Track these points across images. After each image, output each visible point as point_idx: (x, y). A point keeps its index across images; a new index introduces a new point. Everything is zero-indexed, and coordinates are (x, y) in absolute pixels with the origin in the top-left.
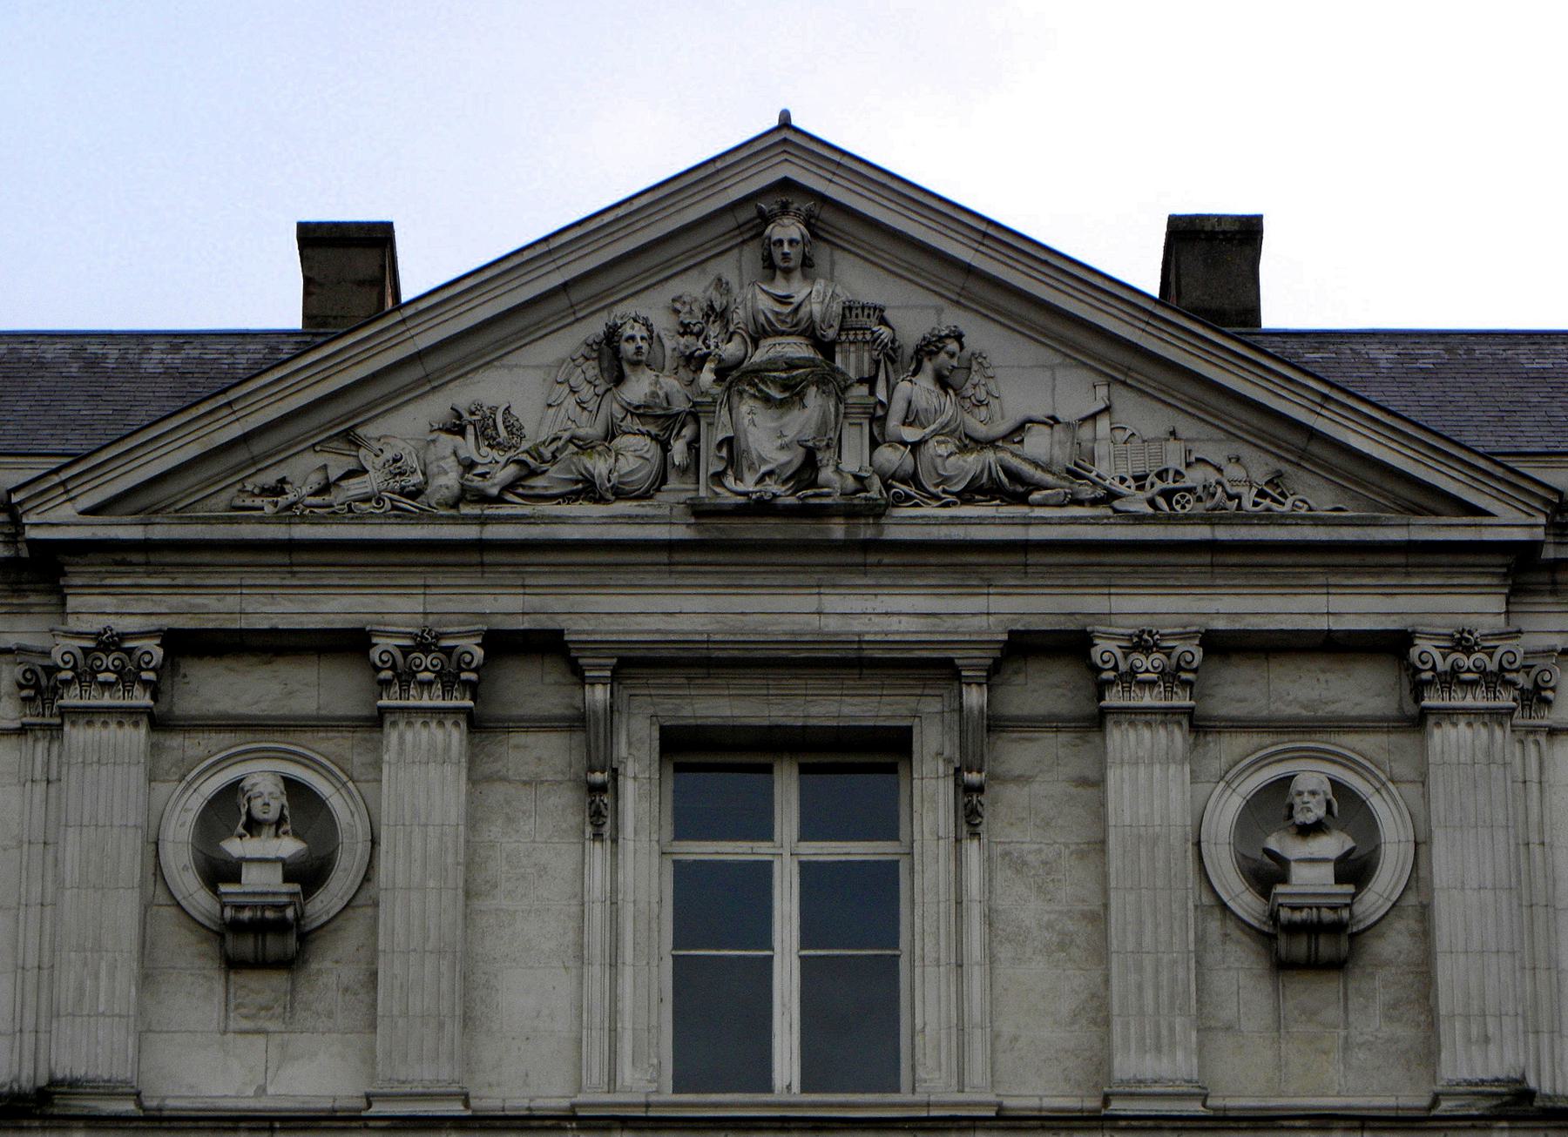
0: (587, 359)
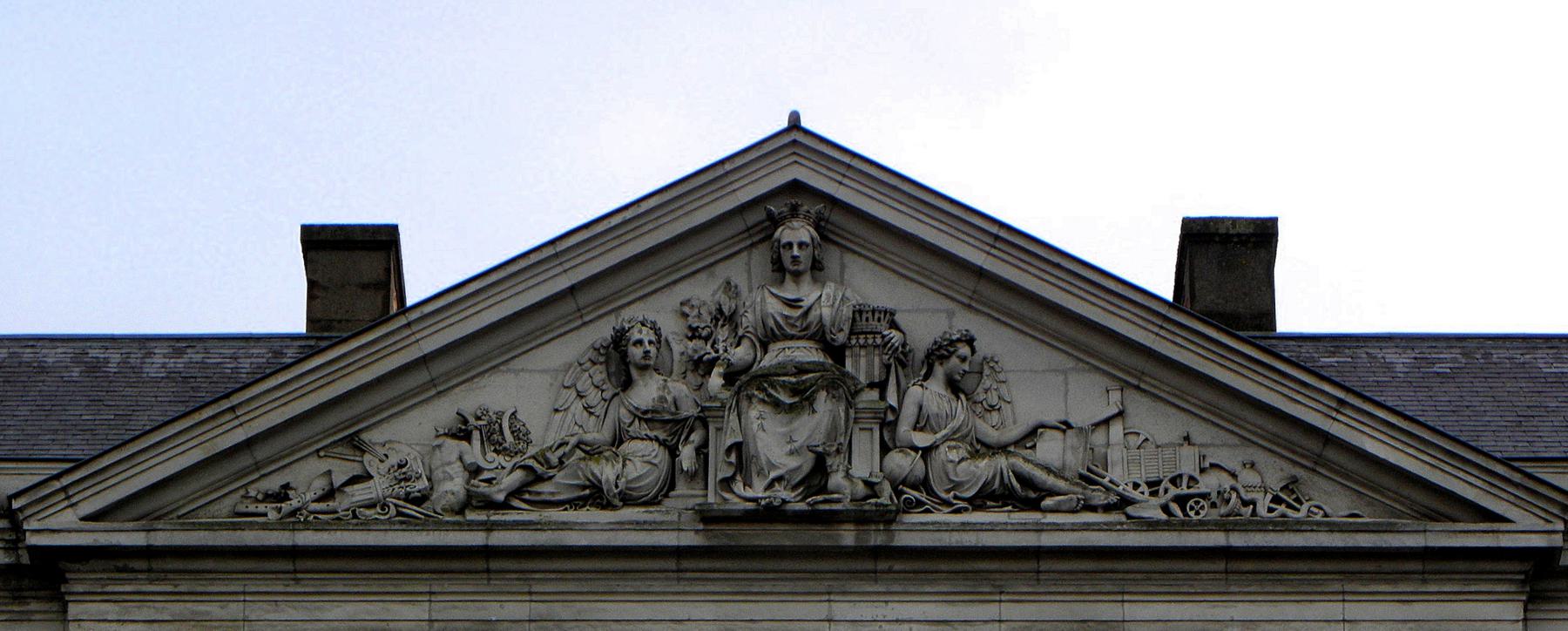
0: (594, 363)
